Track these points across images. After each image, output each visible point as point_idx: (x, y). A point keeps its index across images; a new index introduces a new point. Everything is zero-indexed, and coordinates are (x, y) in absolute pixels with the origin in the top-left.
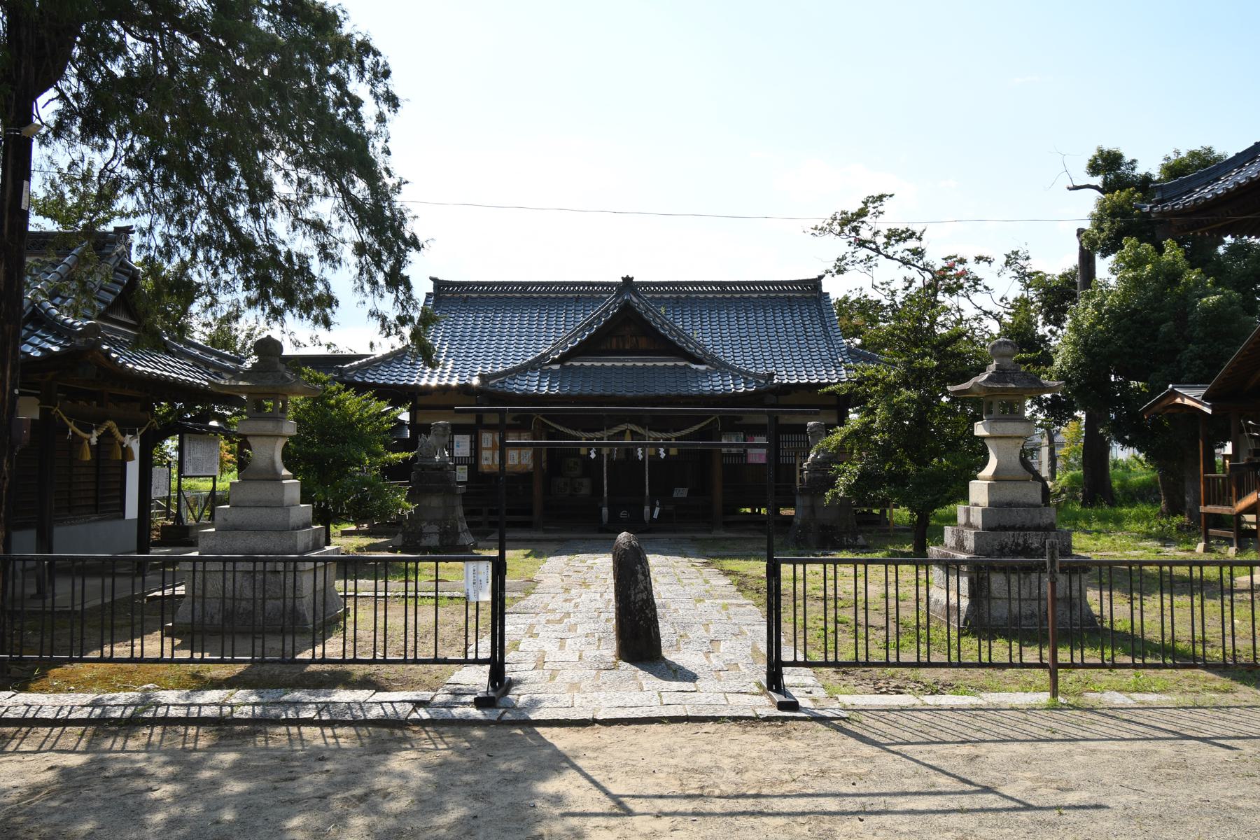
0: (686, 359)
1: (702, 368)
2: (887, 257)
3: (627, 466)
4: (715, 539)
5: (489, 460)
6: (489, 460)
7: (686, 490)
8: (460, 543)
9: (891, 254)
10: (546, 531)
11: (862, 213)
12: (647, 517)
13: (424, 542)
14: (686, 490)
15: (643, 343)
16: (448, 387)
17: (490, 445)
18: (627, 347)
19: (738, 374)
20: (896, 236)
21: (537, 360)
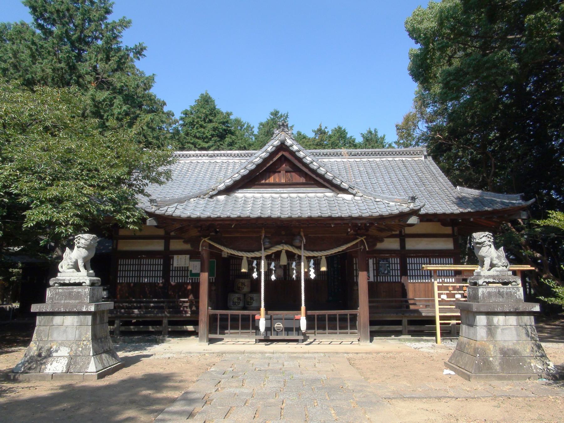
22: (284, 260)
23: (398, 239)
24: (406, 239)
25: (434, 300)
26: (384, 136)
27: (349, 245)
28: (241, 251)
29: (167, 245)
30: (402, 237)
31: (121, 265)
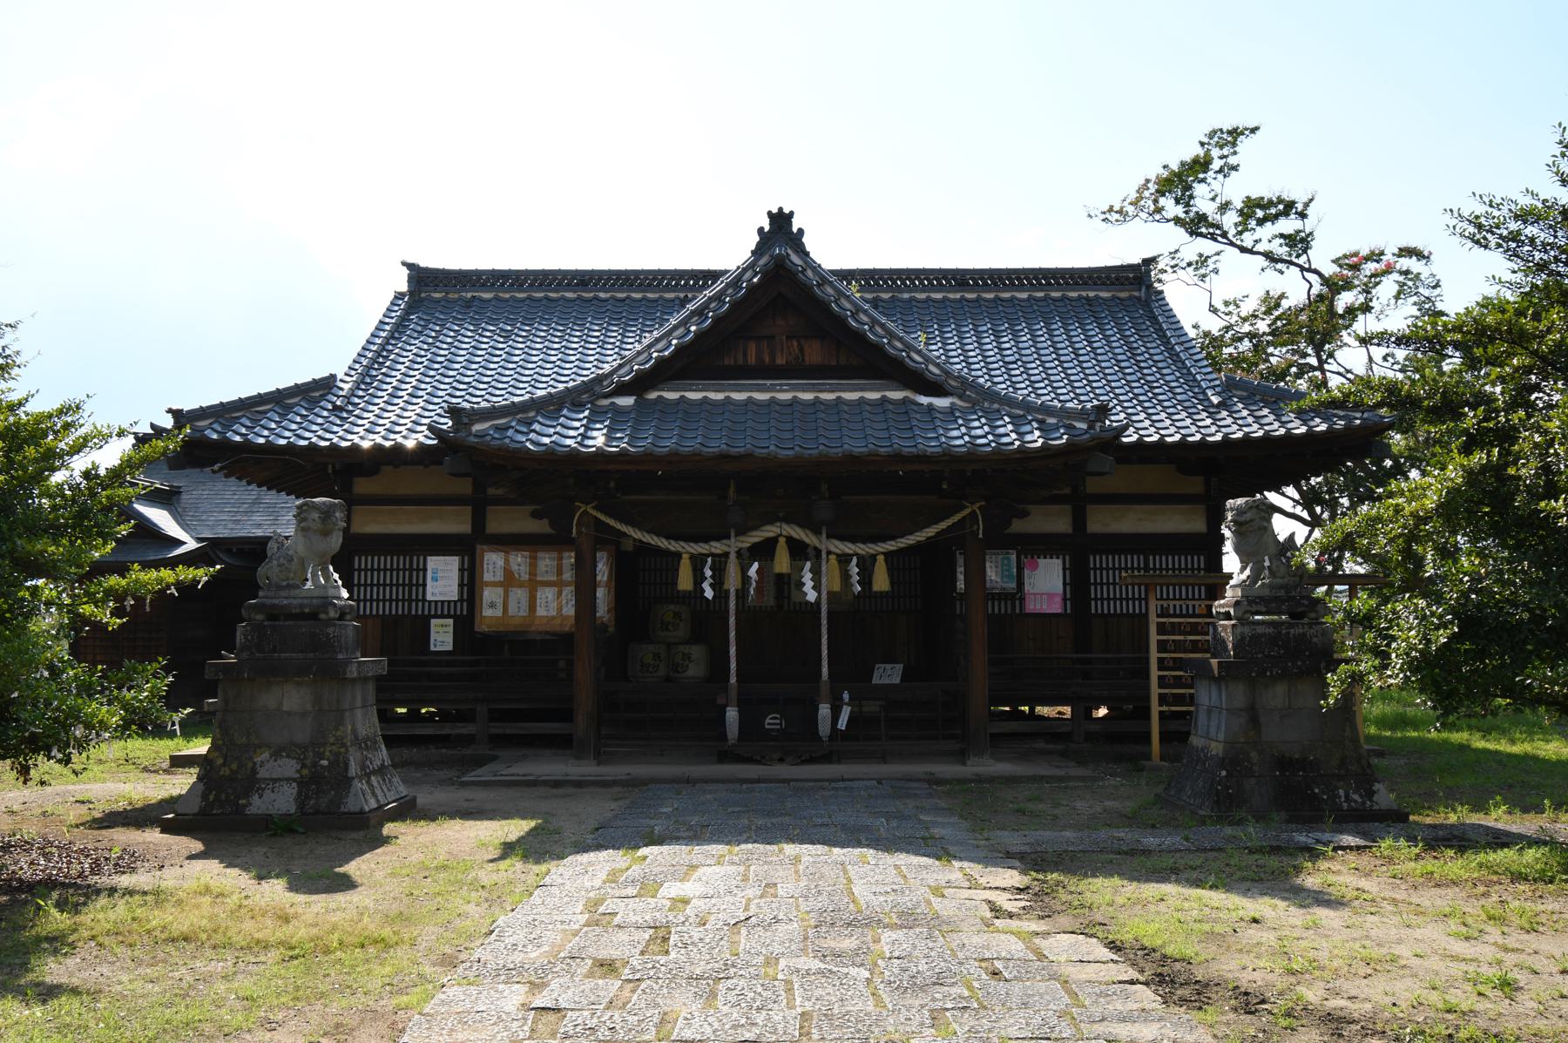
0: (906, 385)
1: (942, 402)
2: (1243, 250)
3: (779, 622)
4: (979, 779)
5: (493, 606)
6: (493, 606)
7: (899, 667)
8: (351, 805)
9: (1248, 243)
10: (600, 757)
11: (1199, 166)
12: (824, 729)
13: (258, 805)
14: (899, 667)
15: (814, 353)
16: (398, 448)
17: (499, 577)
18: (780, 361)
19: (1023, 412)
20: (1257, 210)
21: (586, 387)
22: (782, 563)
23: (1068, 508)
24: (1090, 508)
25: (1147, 659)
26: (170, 411)
27: (943, 525)
28: (677, 539)
29: (1079, 520)
30: (1079, 506)
31: (1096, 599)
